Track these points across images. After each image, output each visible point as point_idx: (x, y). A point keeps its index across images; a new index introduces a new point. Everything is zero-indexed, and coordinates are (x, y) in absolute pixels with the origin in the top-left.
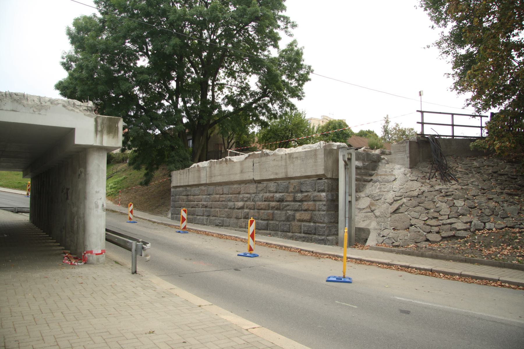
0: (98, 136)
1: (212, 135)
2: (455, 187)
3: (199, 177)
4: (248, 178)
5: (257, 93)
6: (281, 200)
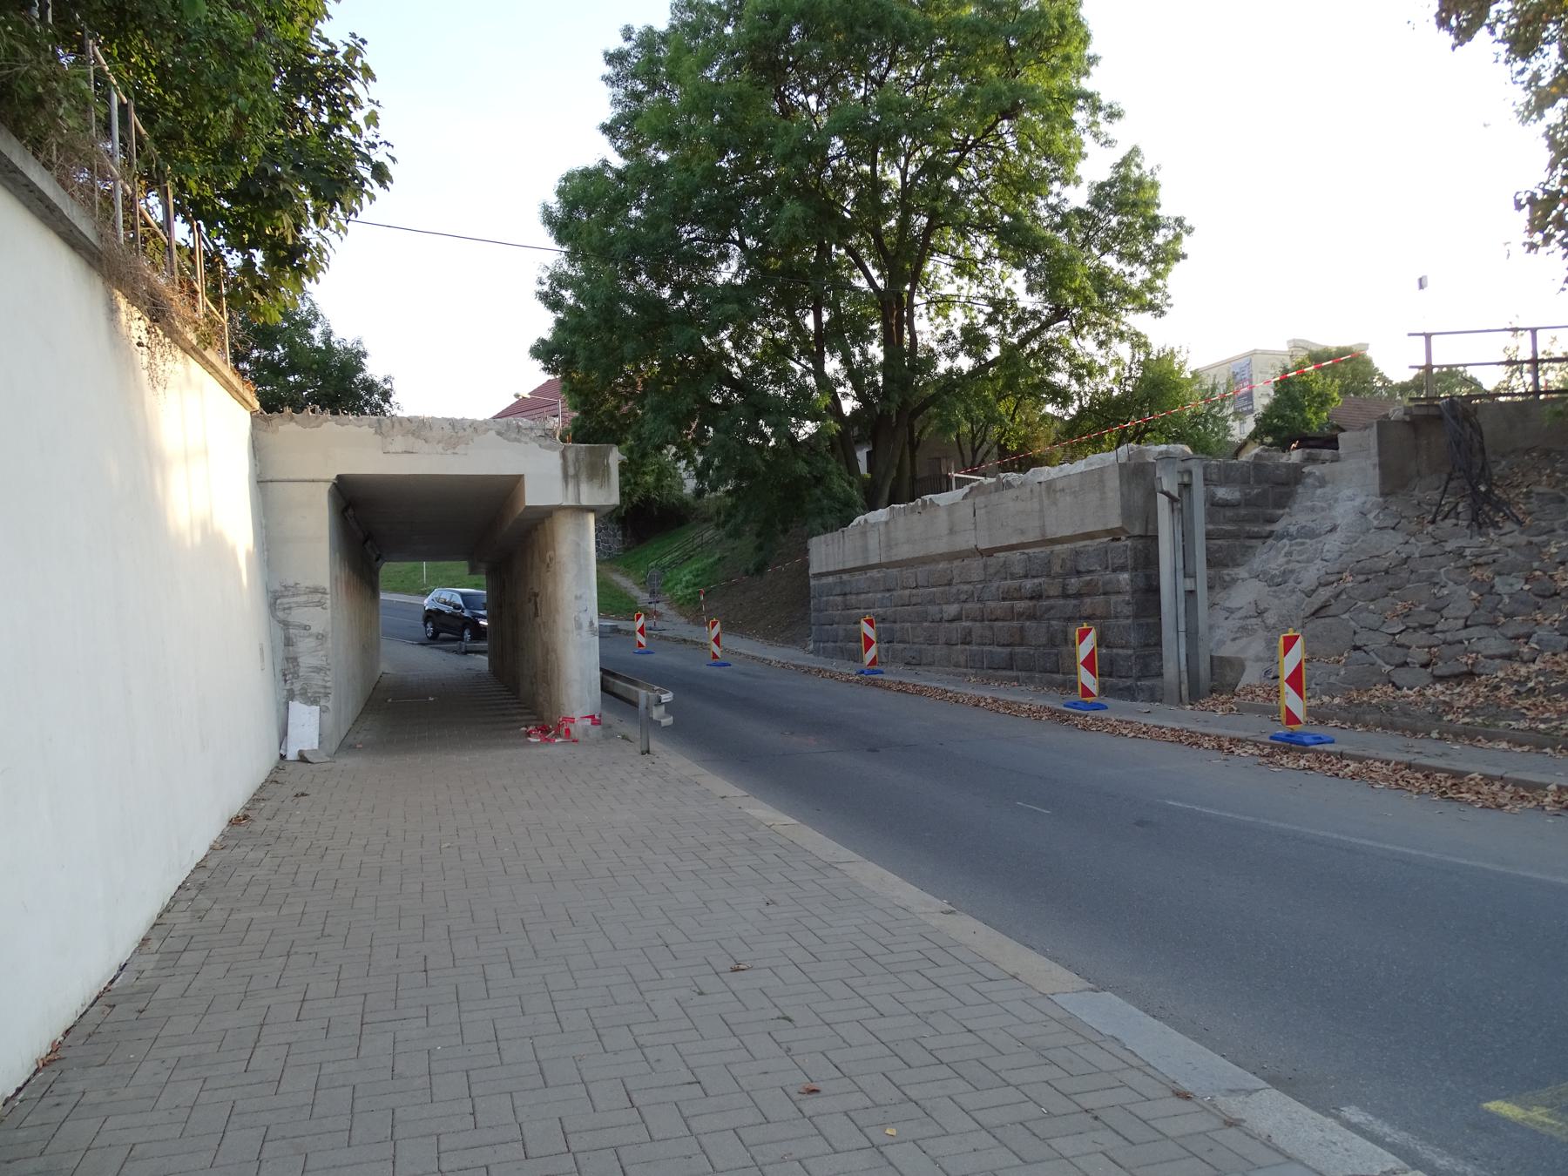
0: (571, 487)
1: (924, 438)
2: (1508, 540)
3: (865, 549)
4: (964, 547)
5: (1035, 314)
6: (1037, 596)
